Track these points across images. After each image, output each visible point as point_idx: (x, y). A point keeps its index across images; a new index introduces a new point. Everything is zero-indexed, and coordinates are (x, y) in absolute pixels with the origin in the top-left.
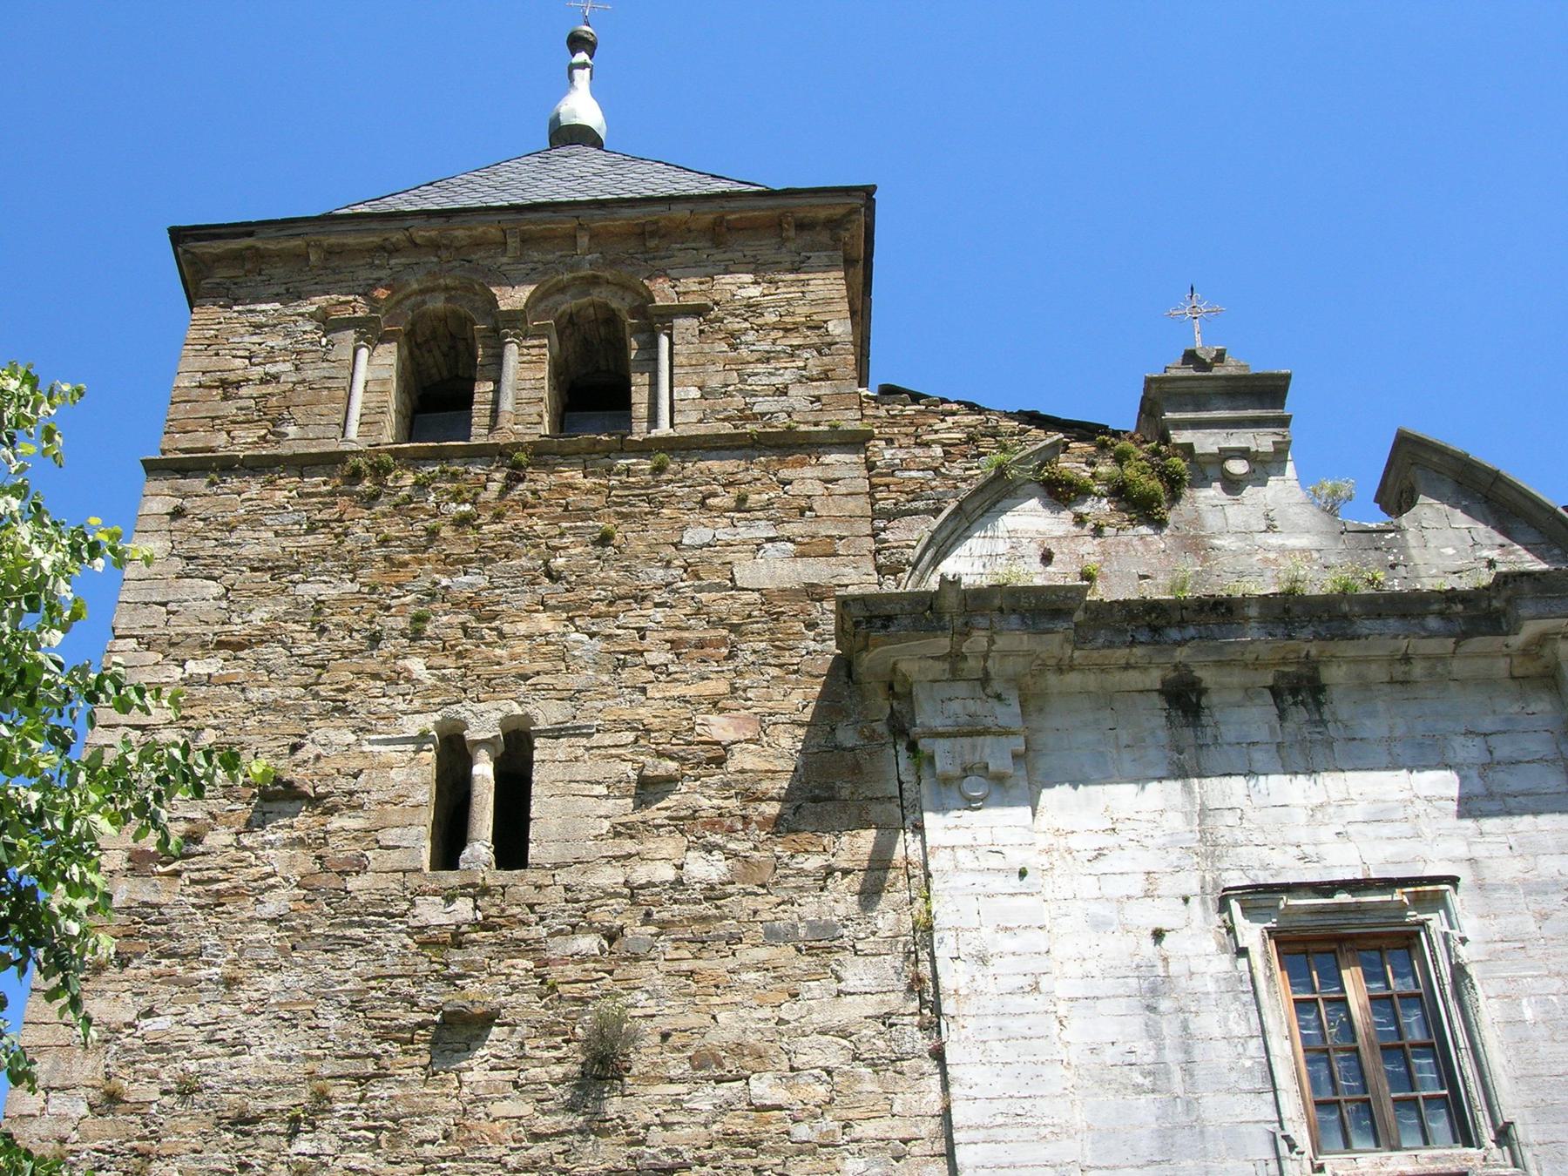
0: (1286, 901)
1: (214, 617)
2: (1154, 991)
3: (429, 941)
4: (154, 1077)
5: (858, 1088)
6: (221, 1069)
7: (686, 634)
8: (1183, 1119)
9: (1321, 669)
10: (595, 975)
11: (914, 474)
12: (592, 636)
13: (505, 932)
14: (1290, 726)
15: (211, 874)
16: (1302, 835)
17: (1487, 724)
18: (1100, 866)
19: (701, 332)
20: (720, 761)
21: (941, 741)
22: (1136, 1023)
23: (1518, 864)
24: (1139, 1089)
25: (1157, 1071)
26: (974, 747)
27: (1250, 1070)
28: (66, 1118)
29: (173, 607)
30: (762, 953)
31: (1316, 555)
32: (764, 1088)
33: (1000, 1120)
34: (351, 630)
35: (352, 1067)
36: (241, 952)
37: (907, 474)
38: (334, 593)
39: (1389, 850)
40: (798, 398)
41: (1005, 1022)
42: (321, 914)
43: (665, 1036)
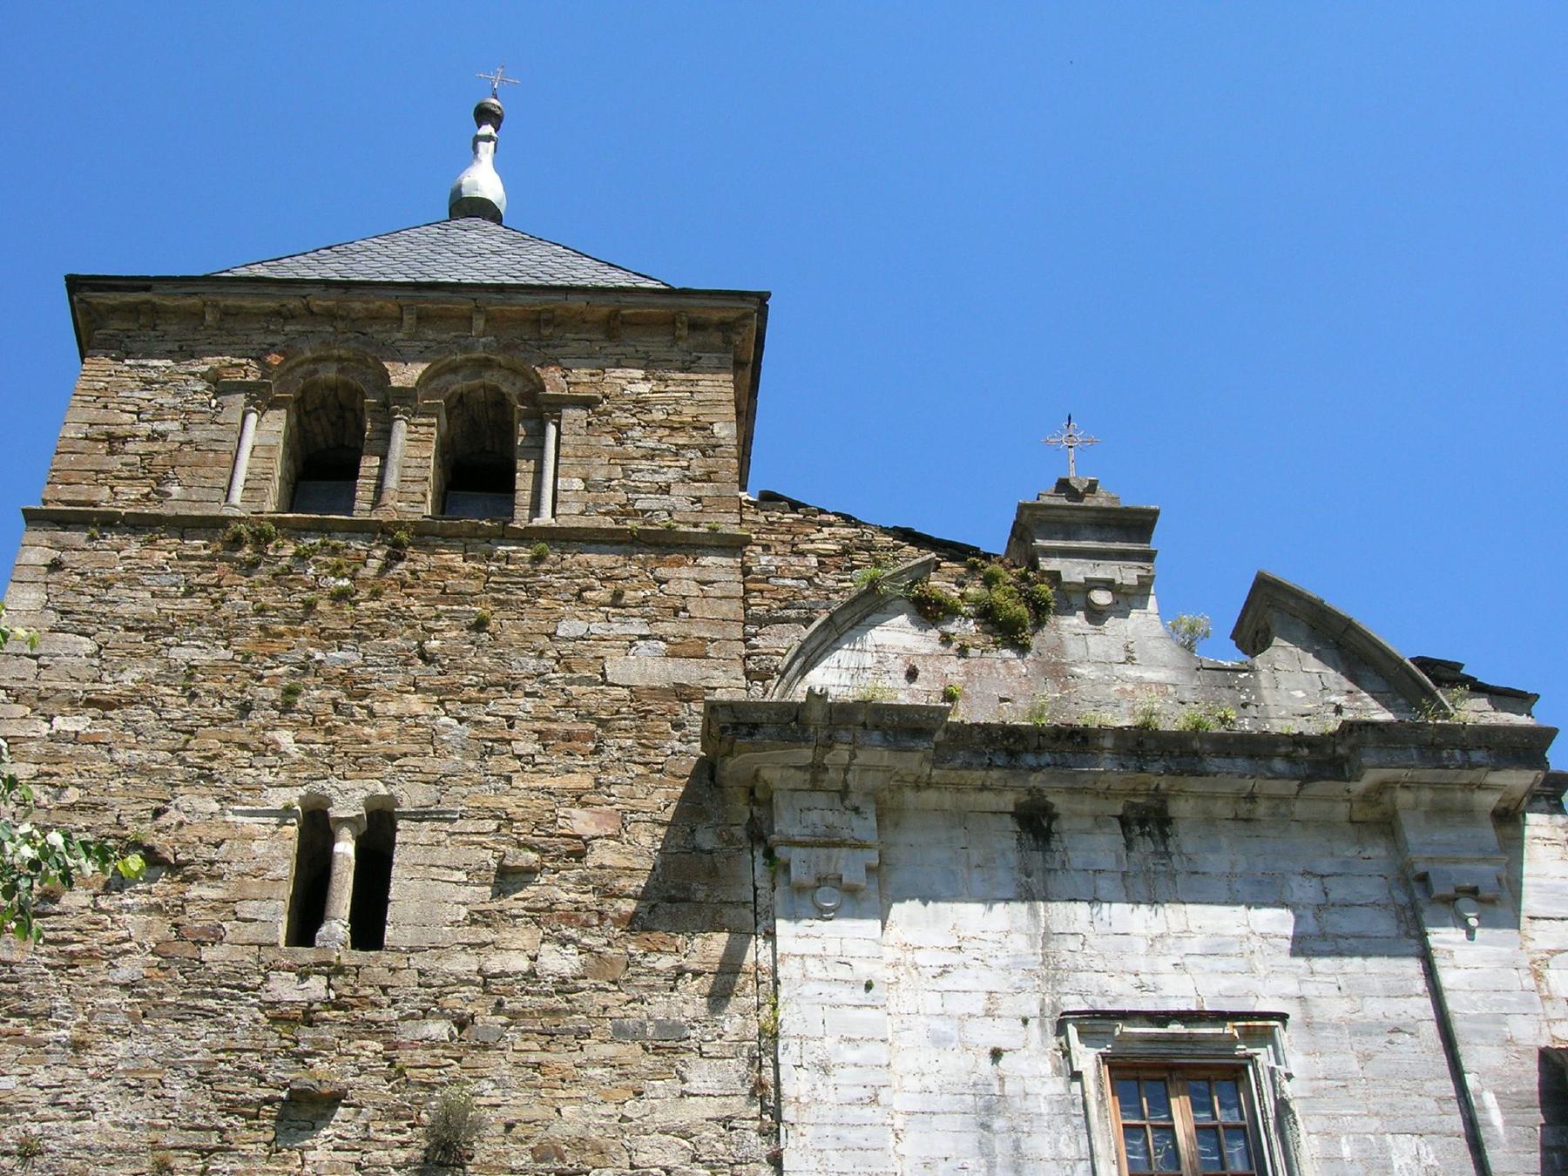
3: (280, 1017)
12: (461, 720)
14: (1136, 856)
15: (66, 935)
16: (1142, 964)
17: (1324, 866)
18: (944, 983)
19: (589, 424)
20: (579, 855)
22: (969, 1140)
31: (1171, 689)
35: (195, 1138)
36: (91, 1015)
39: (1224, 984)
40: (680, 498)
41: (843, 1132)
43: (509, 1127)
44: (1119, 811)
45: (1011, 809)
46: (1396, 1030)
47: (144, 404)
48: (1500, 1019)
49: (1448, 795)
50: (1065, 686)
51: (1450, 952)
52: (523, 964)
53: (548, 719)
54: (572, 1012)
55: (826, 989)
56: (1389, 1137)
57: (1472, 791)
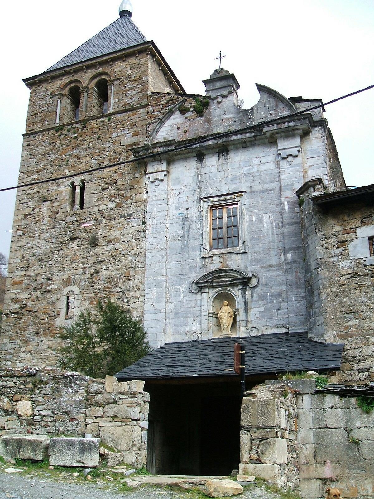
0: (212, 199)
1: (35, 167)
2: (185, 220)
3: (69, 225)
4: (29, 254)
5: (132, 244)
6: (38, 251)
7: (111, 157)
8: (186, 245)
9: (228, 147)
10: (93, 228)
11: (155, 113)
12: (96, 160)
13: (80, 222)
14: (220, 161)
15: (35, 217)
16: (218, 185)
17: (261, 155)
18: (180, 196)
19: (119, 84)
20: (115, 183)
21: (151, 174)
22: (181, 227)
23: (260, 186)
24: (179, 240)
25: (183, 237)
26: (157, 175)
27: (199, 235)
28: (17, 263)
29: (28, 165)
30: (119, 221)
31: (233, 119)
32: (118, 246)
33: (154, 248)
34: (57, 165)
35: (57, 249)
36: (41, 231)
37: (154, 113)
38: (54, 158)
39: (234, 186)
40: (136, 99)
41: (157, 229)
42: (52, 222)
43: (103, 238)
44: (218, 151)
45: (196, 155)
46: (270, 190)
47: (40, 104)
48: (292, 185)
49: (289, 133)
50: (210, 124)
51: (284, 171)
52: (105, 207)
53: (110, 156)
54: (114, 214)
55: (156, 202)
56: (264, 214)
57: (294, 131)
